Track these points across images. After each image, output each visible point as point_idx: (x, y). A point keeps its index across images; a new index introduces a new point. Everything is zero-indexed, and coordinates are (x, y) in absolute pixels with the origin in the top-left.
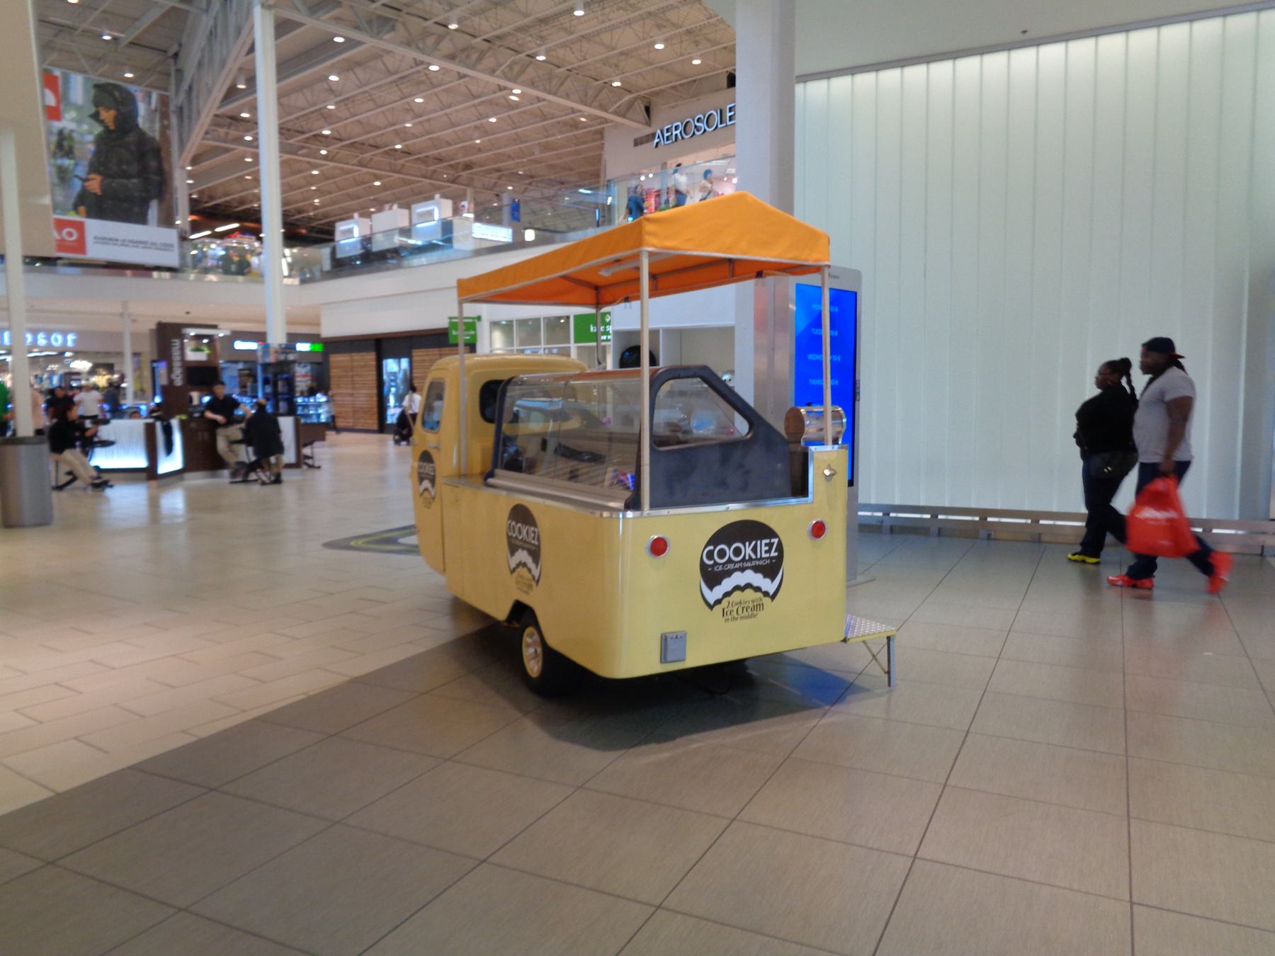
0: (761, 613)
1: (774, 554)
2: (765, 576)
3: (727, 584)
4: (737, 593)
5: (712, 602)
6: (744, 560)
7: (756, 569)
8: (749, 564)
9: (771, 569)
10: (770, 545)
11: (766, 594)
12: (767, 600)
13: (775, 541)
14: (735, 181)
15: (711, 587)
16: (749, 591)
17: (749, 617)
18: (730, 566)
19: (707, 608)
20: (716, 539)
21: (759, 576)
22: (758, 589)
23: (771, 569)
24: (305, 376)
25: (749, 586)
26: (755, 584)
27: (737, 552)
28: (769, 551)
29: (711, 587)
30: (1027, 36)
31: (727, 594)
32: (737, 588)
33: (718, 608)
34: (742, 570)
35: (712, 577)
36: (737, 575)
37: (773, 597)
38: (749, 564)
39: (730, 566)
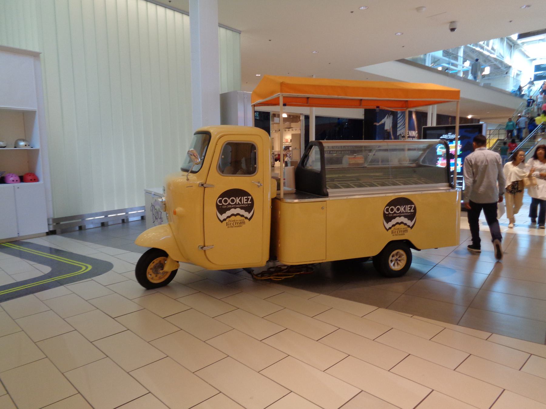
0: (244, 225)
1: (412, 211)
2: (409, 219)
3: (394, 222)
4: (233, 217)
5: (388, 228)
6: (400, 213)
7: (405, 217)
8: (238, 206)
9: (411, 217)
10: (411, 207)
11: (409, 226)
12: (409, 229)
13: (413, 206)
14: (495, 48)
15: (387, 223)
16: (238, 217)
17: (238, 226)
18: (229, 206)
19: (386, 231)
20: (389, 204)
21: (406, 219)
22: (405, 224)
23: (411, 217)
24: (541, 98)
25: (402, 223)
26: (405, 222)
27: (398, 209)
28: (247, 201)
29: (387, 223)
30: (171, 4)
31: (394, 225)
32: (397, 223)
33: (390, 231)
34: (400, 216)
35: (221, 210)
36: (397, 218)
37: (412, 228)
38: (238, 206)
39: (229, 206)
